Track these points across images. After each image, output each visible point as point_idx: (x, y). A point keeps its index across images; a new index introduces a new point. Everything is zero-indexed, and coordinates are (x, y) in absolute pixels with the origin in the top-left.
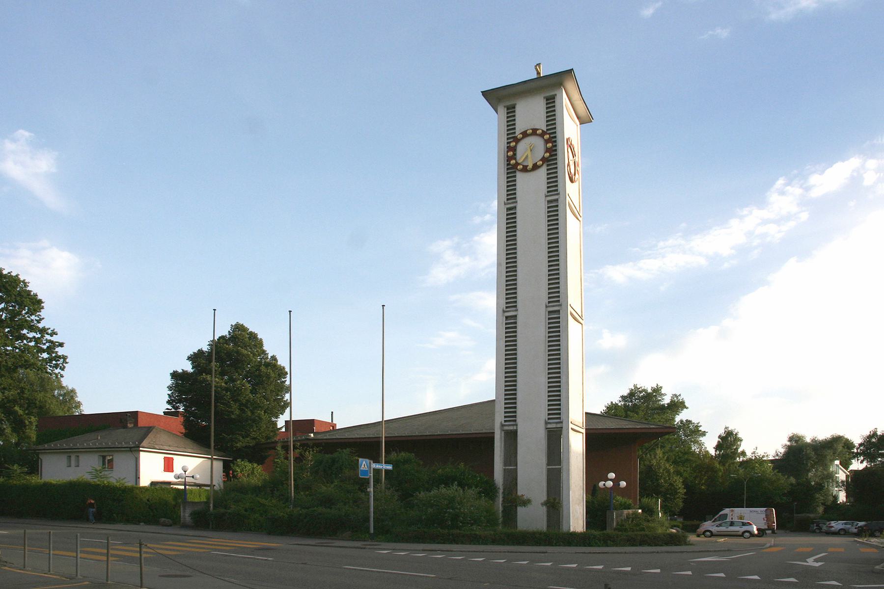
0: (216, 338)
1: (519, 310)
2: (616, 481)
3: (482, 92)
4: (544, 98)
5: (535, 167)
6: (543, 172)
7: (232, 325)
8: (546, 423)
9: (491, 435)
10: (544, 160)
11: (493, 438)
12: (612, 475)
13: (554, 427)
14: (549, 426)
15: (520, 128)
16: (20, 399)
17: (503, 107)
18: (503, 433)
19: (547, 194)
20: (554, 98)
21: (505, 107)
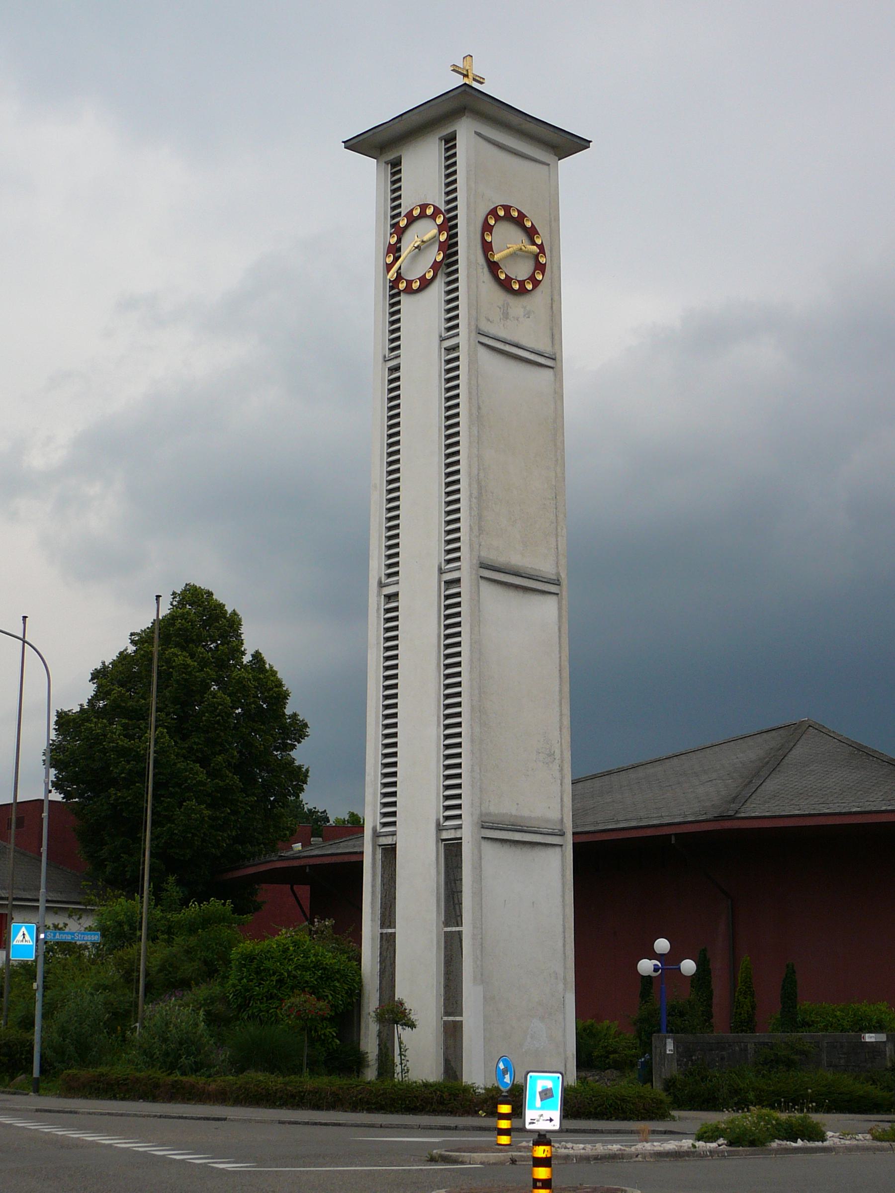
0: (160, 617)
1: (462, 570)
2: (670, 961)
3: (343, 142)
4: (441, 139)
5: (425, 283)
6: (438, 289)
7: (174, 594)
8: (440, 828)
9: (354, 859)
10: (436, 266)
11: (361, 863)
12: (662, 945)
13: (452, 836)
14: (445, 835)
15: (408, 202)
16: (167, 715)
17: (384, 164)
18: (379, 851)
19: (445, 334)
20: (455, 139)
21: (387, 163)
